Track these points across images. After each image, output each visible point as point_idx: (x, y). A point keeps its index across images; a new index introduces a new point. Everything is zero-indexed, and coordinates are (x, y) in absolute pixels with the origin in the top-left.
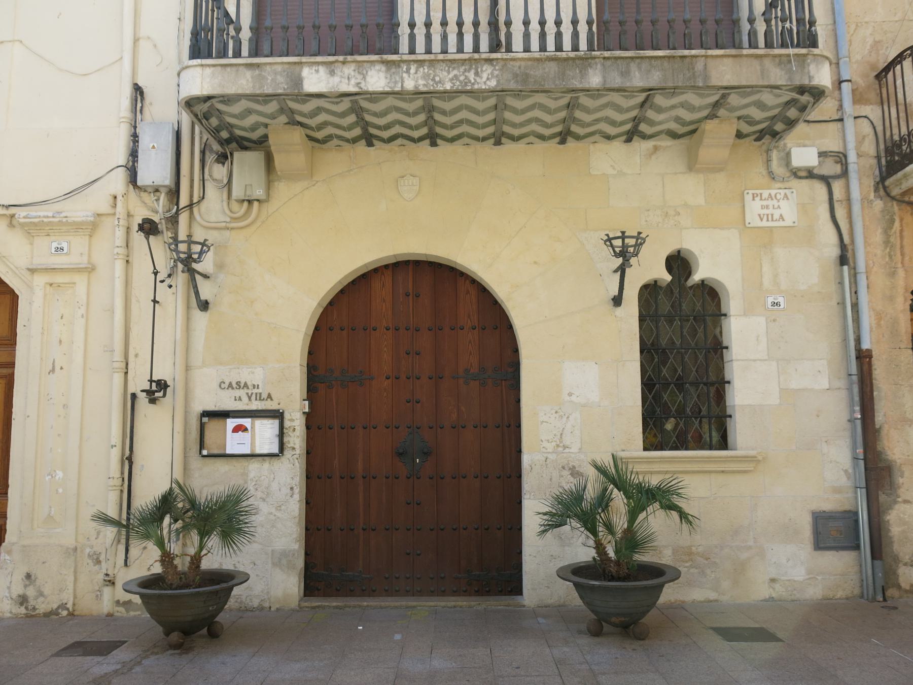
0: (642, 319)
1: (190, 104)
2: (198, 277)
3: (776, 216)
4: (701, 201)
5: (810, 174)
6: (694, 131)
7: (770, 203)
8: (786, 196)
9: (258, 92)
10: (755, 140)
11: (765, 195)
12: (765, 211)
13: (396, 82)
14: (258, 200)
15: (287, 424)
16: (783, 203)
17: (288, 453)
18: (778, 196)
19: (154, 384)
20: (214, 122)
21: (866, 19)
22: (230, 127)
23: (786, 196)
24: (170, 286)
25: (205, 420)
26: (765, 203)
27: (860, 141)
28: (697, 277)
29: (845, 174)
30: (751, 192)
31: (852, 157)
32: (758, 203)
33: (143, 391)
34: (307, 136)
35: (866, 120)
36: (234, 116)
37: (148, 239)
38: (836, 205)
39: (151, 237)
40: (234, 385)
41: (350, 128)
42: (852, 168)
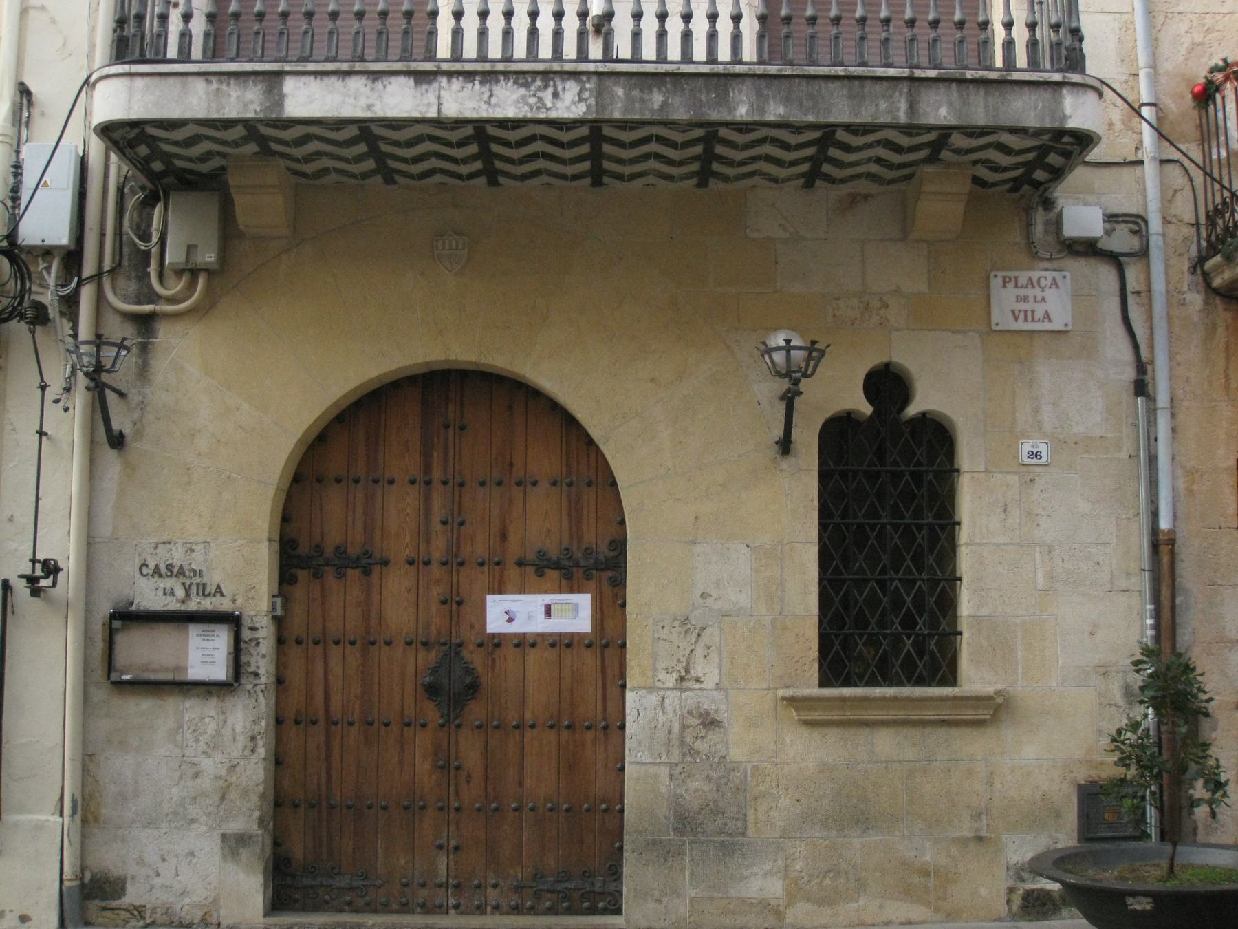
0: (824, 476)
1: (107, 131)
2: (111, 396)
3: (1039, 314)
4: (923, 287)
5: (1087, 249)
6: (908, 177)
7: (1030, 292)
8: (1055, 282)
9: (215, 115)
10: (1009, 191)
11: (1023, 279)
12: (1023, 306)
13: (429, 105)
14: (205, 270)
15: (246, 634)
16: (1050, 294)
17: (247, 682)
18: (1043, 283)
19: (38, 566)
20: (143, 150)
21: (1181, 9)
22: (167, 158)
23: (1055, 282)
24: (66, 410)
25: (117, 624)
26: (1022, 292)
27: (1168, 196)
28: (912, 410)
29: (1143, 254)
30: (1000, 274)
31: (1155, 224)
32: (1011, 292)
33: (21, 576)
34: (289, 169)
35: (1177, 166)
36: (176, 143)
37: (33, 332)
38: (1131, 300)
39: (38, 328)
40: (163, 570)
41: (359, 159)
42: (1155, 242)
